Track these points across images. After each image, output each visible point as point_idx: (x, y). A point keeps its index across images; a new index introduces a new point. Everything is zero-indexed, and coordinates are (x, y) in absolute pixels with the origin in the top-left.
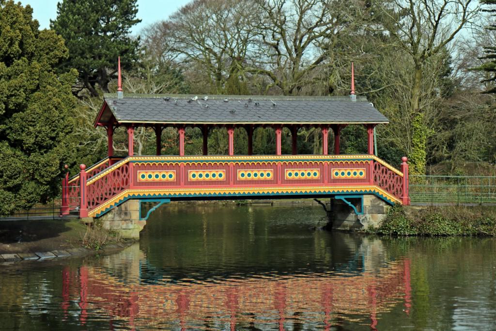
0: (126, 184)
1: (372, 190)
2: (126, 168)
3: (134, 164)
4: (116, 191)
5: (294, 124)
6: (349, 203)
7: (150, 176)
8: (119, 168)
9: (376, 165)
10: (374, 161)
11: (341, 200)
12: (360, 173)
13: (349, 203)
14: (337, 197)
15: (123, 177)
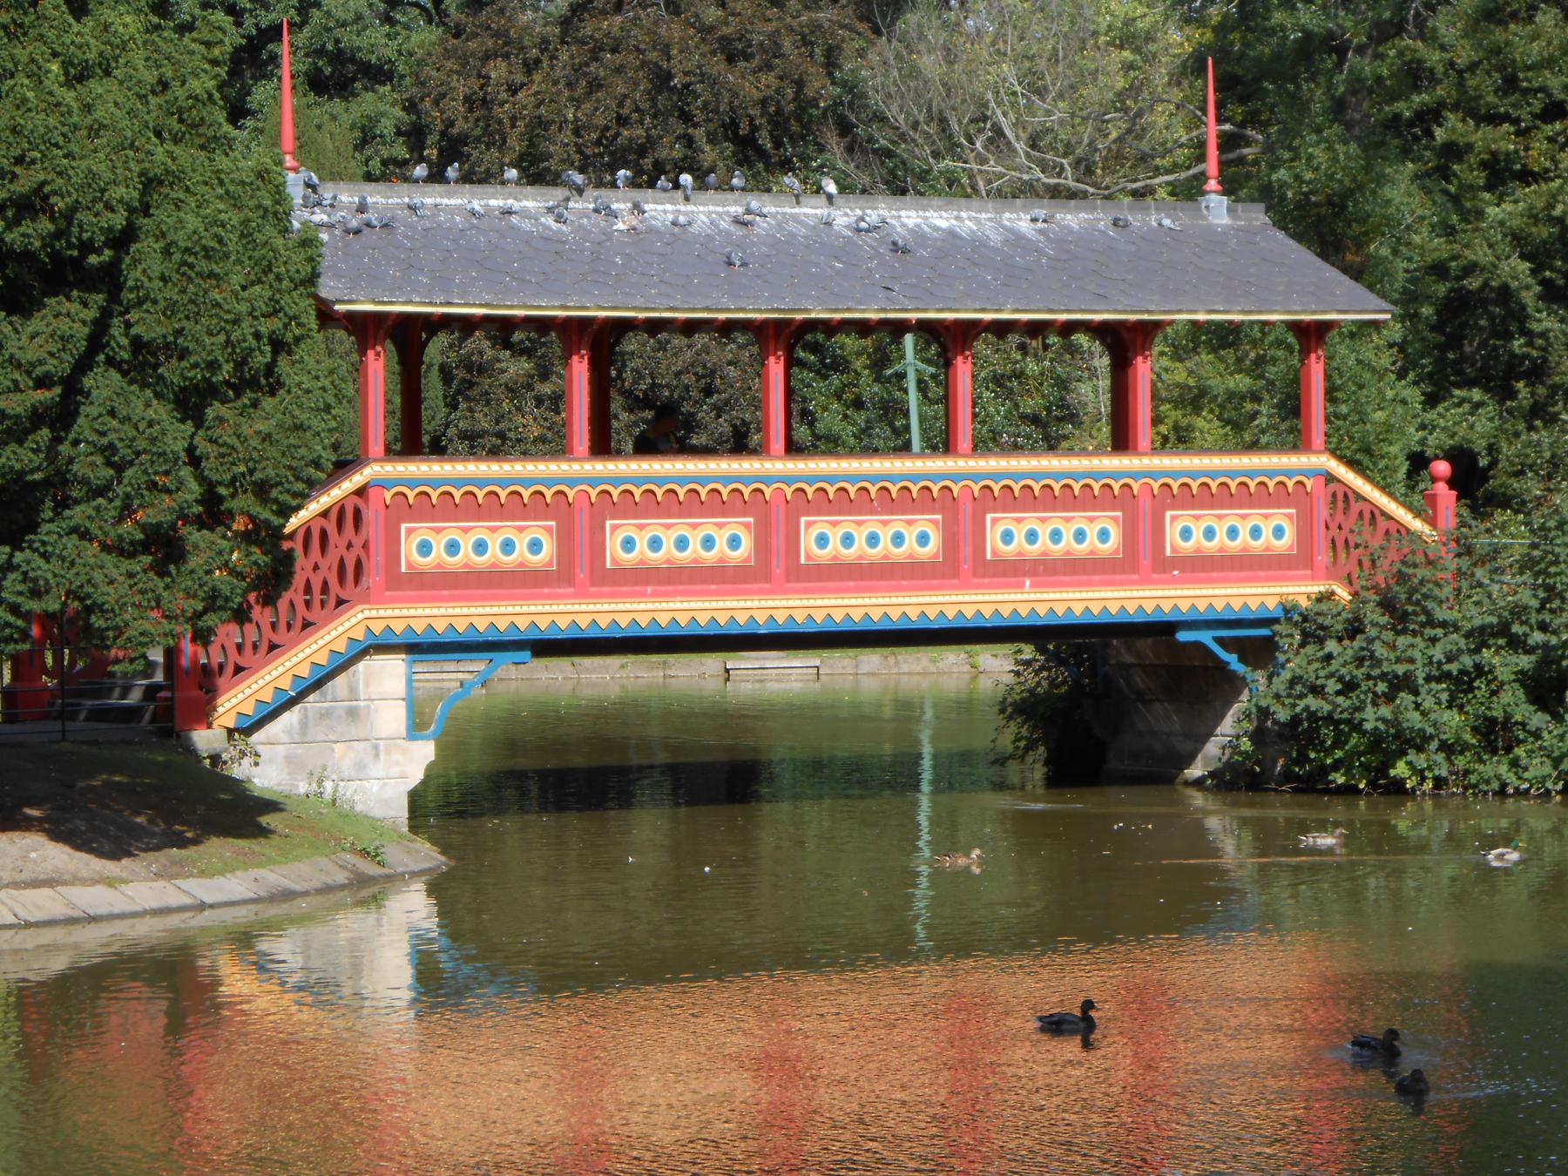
0: (357, 581)
1: (359, 634)
2: (357, 513)
3: (388, 495)
4: (315, 614)
5: (957, 322)
6: (1232, 659)
7: (873, 540)
8: (325, 514)
9: (1334, 495)
10: (1330, 478)
11: (1199, 645)
12: (1273, 530)
13: (1232, 659)
14: (1183, 636)
15: (342, 550)
